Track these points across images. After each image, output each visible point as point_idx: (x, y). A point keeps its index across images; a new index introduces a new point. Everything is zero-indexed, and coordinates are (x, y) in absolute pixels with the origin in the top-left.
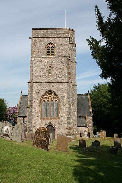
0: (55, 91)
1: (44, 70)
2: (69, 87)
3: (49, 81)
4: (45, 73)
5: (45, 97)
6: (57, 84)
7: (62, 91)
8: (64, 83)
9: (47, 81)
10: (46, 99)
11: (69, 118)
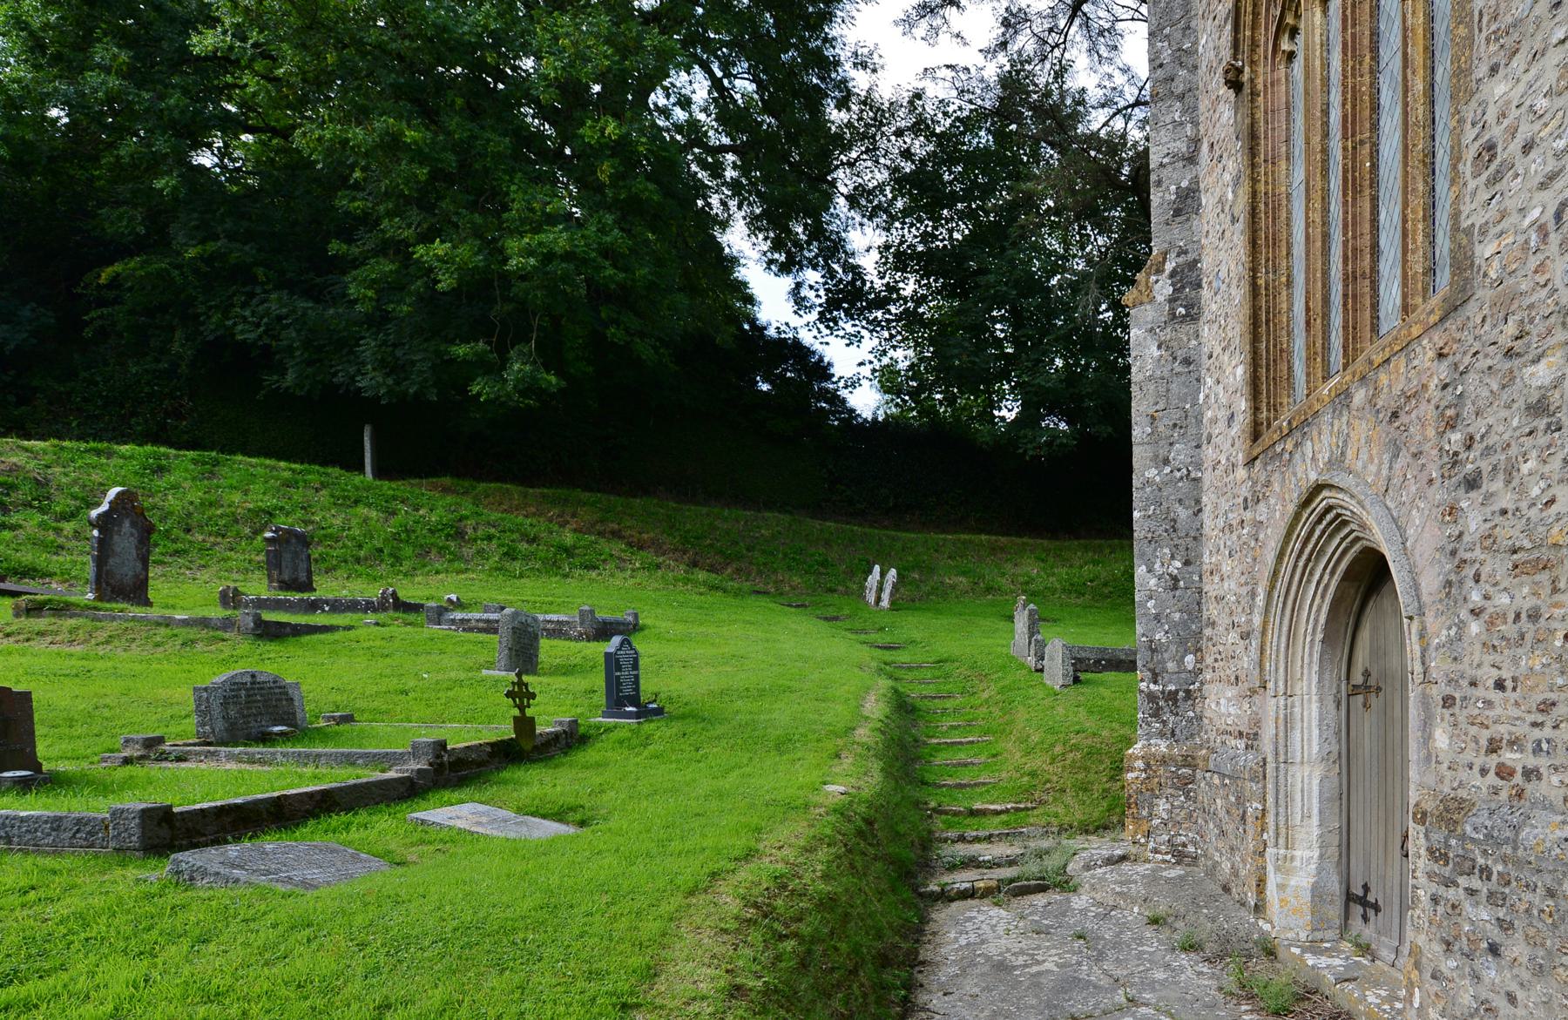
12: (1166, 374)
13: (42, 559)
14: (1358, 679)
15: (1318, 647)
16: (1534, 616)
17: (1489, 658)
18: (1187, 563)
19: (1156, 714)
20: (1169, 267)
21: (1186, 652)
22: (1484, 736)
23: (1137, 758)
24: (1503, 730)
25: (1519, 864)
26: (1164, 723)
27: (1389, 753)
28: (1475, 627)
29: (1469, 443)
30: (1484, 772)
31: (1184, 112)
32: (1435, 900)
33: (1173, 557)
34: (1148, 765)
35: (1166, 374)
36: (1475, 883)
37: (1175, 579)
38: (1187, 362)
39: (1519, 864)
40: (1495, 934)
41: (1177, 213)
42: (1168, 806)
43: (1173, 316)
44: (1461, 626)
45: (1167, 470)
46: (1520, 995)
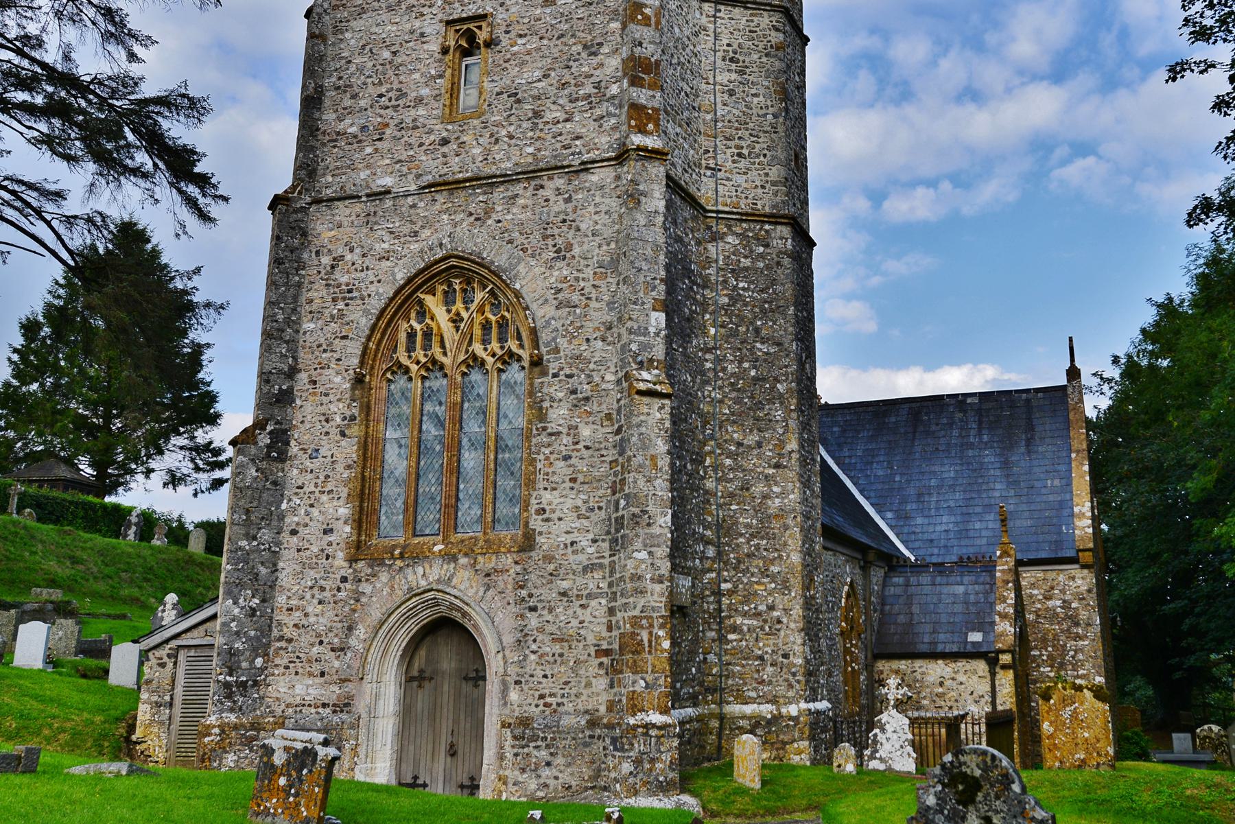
0: (499, 257)
1: (416, 76)
2: (633, 198)
3: (456, 167)
4: (419, 101)
5: (411, 336)
6: (518, 188)
7: (561, 254)
8: (585, 167)
9: (432, 167)
10: (420, 354)
11: (617, 535)
12: (260, 486)
13: (472, 604)
14: (415, 673)
15: (398, 658)
16: (561, 655)
17: (539, 668)
18: (263, 601)
19: (229, 696)
20: (269, 428)
21: (257, 656)
22: (537, 694)
23: (215, 727)
24: (547, 691)
25: (559, 732)
26: (234, 702)
27: (438, 709)
28: (533, 657)
29: (530, 595)
30: (537, 706)
31: (288, 351)
32: (516, 755)
33: (253, 596)
34: (223, 731)
35: (260, 486)
36: (540, 743)
37: (253, 610)
38: (275, 483)
39: (559, 732)
40: (549, 758)
41: (278, 401)
42: (236, 758)
43: (268, 455)
44: (526, 656)
45: (255, 543)
46: (560, 775)
